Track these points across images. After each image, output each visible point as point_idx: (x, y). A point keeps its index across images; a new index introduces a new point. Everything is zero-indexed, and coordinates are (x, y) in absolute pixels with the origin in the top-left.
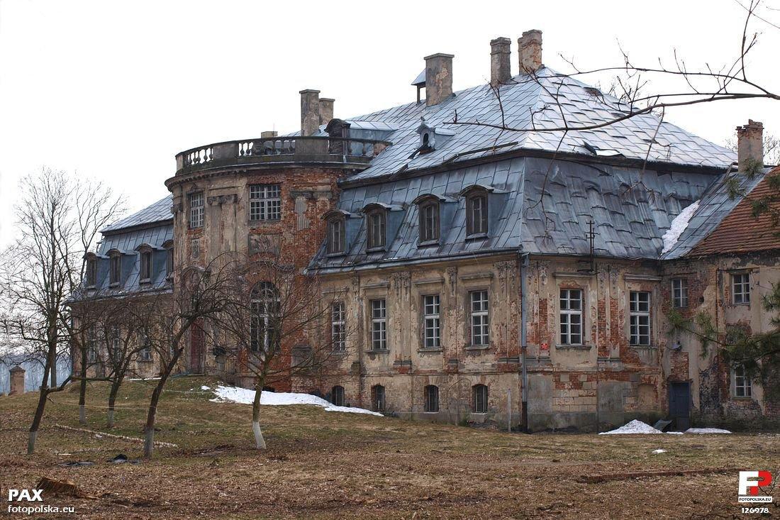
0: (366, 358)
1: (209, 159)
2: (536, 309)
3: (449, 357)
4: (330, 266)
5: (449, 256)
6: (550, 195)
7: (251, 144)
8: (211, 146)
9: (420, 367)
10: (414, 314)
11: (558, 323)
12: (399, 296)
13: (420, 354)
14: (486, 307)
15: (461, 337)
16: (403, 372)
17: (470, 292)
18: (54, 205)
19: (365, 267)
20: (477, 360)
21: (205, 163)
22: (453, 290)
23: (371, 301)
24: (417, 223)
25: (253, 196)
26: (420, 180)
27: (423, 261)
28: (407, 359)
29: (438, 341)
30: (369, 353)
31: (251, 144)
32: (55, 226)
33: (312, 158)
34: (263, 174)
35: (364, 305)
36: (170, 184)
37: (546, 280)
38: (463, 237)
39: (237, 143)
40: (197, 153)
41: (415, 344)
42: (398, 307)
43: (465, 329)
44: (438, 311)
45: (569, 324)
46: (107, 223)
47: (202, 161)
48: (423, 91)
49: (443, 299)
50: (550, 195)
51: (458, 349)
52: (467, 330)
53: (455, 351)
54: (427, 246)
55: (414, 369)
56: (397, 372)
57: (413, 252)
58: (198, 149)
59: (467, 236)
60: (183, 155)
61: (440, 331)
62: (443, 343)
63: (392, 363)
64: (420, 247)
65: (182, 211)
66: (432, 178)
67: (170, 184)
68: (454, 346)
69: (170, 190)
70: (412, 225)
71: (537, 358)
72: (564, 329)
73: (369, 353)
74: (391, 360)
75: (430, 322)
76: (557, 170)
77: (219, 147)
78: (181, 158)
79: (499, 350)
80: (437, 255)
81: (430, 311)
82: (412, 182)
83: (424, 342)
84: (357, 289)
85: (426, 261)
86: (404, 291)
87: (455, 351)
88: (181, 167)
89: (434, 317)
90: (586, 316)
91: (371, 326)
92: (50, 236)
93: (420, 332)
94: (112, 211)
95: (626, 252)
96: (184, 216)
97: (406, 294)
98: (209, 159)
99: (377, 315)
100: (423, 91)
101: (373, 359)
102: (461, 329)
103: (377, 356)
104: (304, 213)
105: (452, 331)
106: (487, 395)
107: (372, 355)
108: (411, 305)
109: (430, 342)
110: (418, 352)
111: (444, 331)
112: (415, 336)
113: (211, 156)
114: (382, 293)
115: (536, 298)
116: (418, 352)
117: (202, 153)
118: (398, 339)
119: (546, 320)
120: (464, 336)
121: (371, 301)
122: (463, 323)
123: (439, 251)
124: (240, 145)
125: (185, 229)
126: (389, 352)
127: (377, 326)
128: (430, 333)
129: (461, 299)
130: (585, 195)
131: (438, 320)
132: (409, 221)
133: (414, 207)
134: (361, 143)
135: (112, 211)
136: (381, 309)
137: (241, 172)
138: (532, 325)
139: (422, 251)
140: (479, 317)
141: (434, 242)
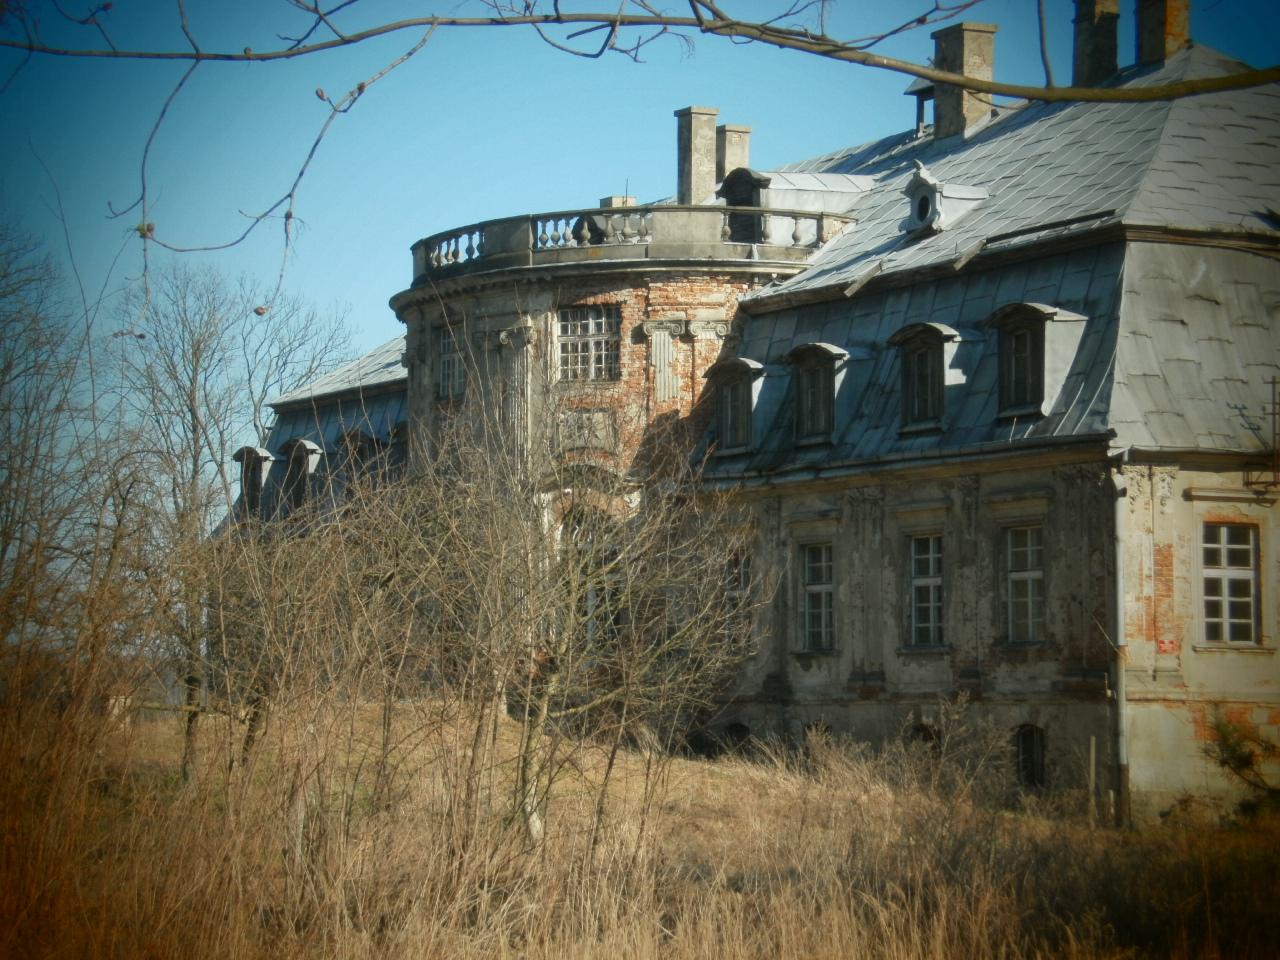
0: (794, 667)
1: (476, 254)
2: (1148, 565)
3: (962, 665)
4: (721, 475)
5: (960, 455)
6: (1183, 323)
7: (476, 238)
8: (482, 227)
9: (901, 687)
10: (889, 575)
11: (1199, 598)
12: (860, 537)
13: (902, 658)
14: (1040, 564)
15: (987, 624)
16: (868, 694)
17: (1005, 529)
18: (197, 353)
19: (791, 478)
20: (1022, 671)
21: (470, 261)
22: (970, 525)
23: (802, 547)
24: (898, 386)
25: (687, 323)
26: (906, 297)
27: (907, 465)
28: (876, 669)
29: (940, 631)
30: (800, 657)
31: (476, 238)
32: (199, 395)
33: (687, 249)
34: (585, 285)
35: (789, 556)
36: (402, 306)
37: (1169, 502)
38: (991, 414)
39: (534, 220)
40: (453, 242)
41: (890, 641)
42: (857, 562)
43: (994, 608)
44: (939, 570)
45: (1225, 599)
46: (700, 373)
47: (463, 257)
48: (929, 105)
49: (950, 543)
50: (1183, 323)
51: (980, 650)
52: (999, 608)
53: (974, 653)
54: (918, 434)
55: (890, 689)
56: (854, 696)
57: (888, 444)
58: (454, 234)
59: (1000, 411)
60: (424, 248)
61: (944, 611)
62: (949, 637)
63: (844, 678)
64: (902, 436)
65: (423, 361)
66: (932, 290)
67: (402, 306)
68: (972, 644)
69: (401, 317)
70: (887, 389)
71: (1151, 672)
72: (1213, 609)
73: (800, 657)
74: (843, 668)
75: (922, 593)
76: (1202, 267)
77: (496, 229)
78: (422, 252)
79: (1066, 652)
80: (936, 453)
81: (923, 569)
82: (891, 300)
83: (909, 632)
84: (773, 522)
85: (913, 464)
86: (869, 526)
87: (974, 653)
88: (422, 271)
89: (931, 582)
90: (1263, 580)
91: (804, 607)
92: (189, 416)
93: (899, 613)
94: (315, 365)
95: (1153, 443)
96: (427, 371)
97: (875, 532)
98: (476, 254)
99: (816, 577)
100: (929, 105)
101: (807, 668)
102: (985, 607)
103: (814, 664)
104: (670, 365)
105: (967, 610)
106: (1044, 748)
107: (805, 659)
108: (883, 556)
109: (923, 634)
110: (899, 655)
111: (950, 612)
112: (891, 622)
113: (480, 247)
114: (825, 530)
115: (1147, 542)
116: (899, 655)
117: (464, 241)
118: (858, 626)
119: (1170, 589)
120: (993, 623)
121: (802, 547)
122: (991, 594)
123: (939, 445)
124: (540, 224)
125: (429, 398)
126: (839, 654)
127: (815, 598)
128: (923, 614)
129: (985, 546)
130: (1266, 320)
131: (939, 589)
132: (881, 381)
133: (892, 352)
134: (789, 219)
135: (315, 365)
136: (824, 564)
137: (541, 281)
138: (1138, 599)
139: (907, 443)
140: (1024, 583)
141: (930, 425)
